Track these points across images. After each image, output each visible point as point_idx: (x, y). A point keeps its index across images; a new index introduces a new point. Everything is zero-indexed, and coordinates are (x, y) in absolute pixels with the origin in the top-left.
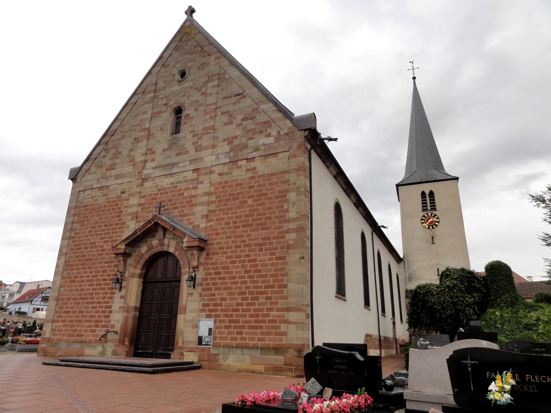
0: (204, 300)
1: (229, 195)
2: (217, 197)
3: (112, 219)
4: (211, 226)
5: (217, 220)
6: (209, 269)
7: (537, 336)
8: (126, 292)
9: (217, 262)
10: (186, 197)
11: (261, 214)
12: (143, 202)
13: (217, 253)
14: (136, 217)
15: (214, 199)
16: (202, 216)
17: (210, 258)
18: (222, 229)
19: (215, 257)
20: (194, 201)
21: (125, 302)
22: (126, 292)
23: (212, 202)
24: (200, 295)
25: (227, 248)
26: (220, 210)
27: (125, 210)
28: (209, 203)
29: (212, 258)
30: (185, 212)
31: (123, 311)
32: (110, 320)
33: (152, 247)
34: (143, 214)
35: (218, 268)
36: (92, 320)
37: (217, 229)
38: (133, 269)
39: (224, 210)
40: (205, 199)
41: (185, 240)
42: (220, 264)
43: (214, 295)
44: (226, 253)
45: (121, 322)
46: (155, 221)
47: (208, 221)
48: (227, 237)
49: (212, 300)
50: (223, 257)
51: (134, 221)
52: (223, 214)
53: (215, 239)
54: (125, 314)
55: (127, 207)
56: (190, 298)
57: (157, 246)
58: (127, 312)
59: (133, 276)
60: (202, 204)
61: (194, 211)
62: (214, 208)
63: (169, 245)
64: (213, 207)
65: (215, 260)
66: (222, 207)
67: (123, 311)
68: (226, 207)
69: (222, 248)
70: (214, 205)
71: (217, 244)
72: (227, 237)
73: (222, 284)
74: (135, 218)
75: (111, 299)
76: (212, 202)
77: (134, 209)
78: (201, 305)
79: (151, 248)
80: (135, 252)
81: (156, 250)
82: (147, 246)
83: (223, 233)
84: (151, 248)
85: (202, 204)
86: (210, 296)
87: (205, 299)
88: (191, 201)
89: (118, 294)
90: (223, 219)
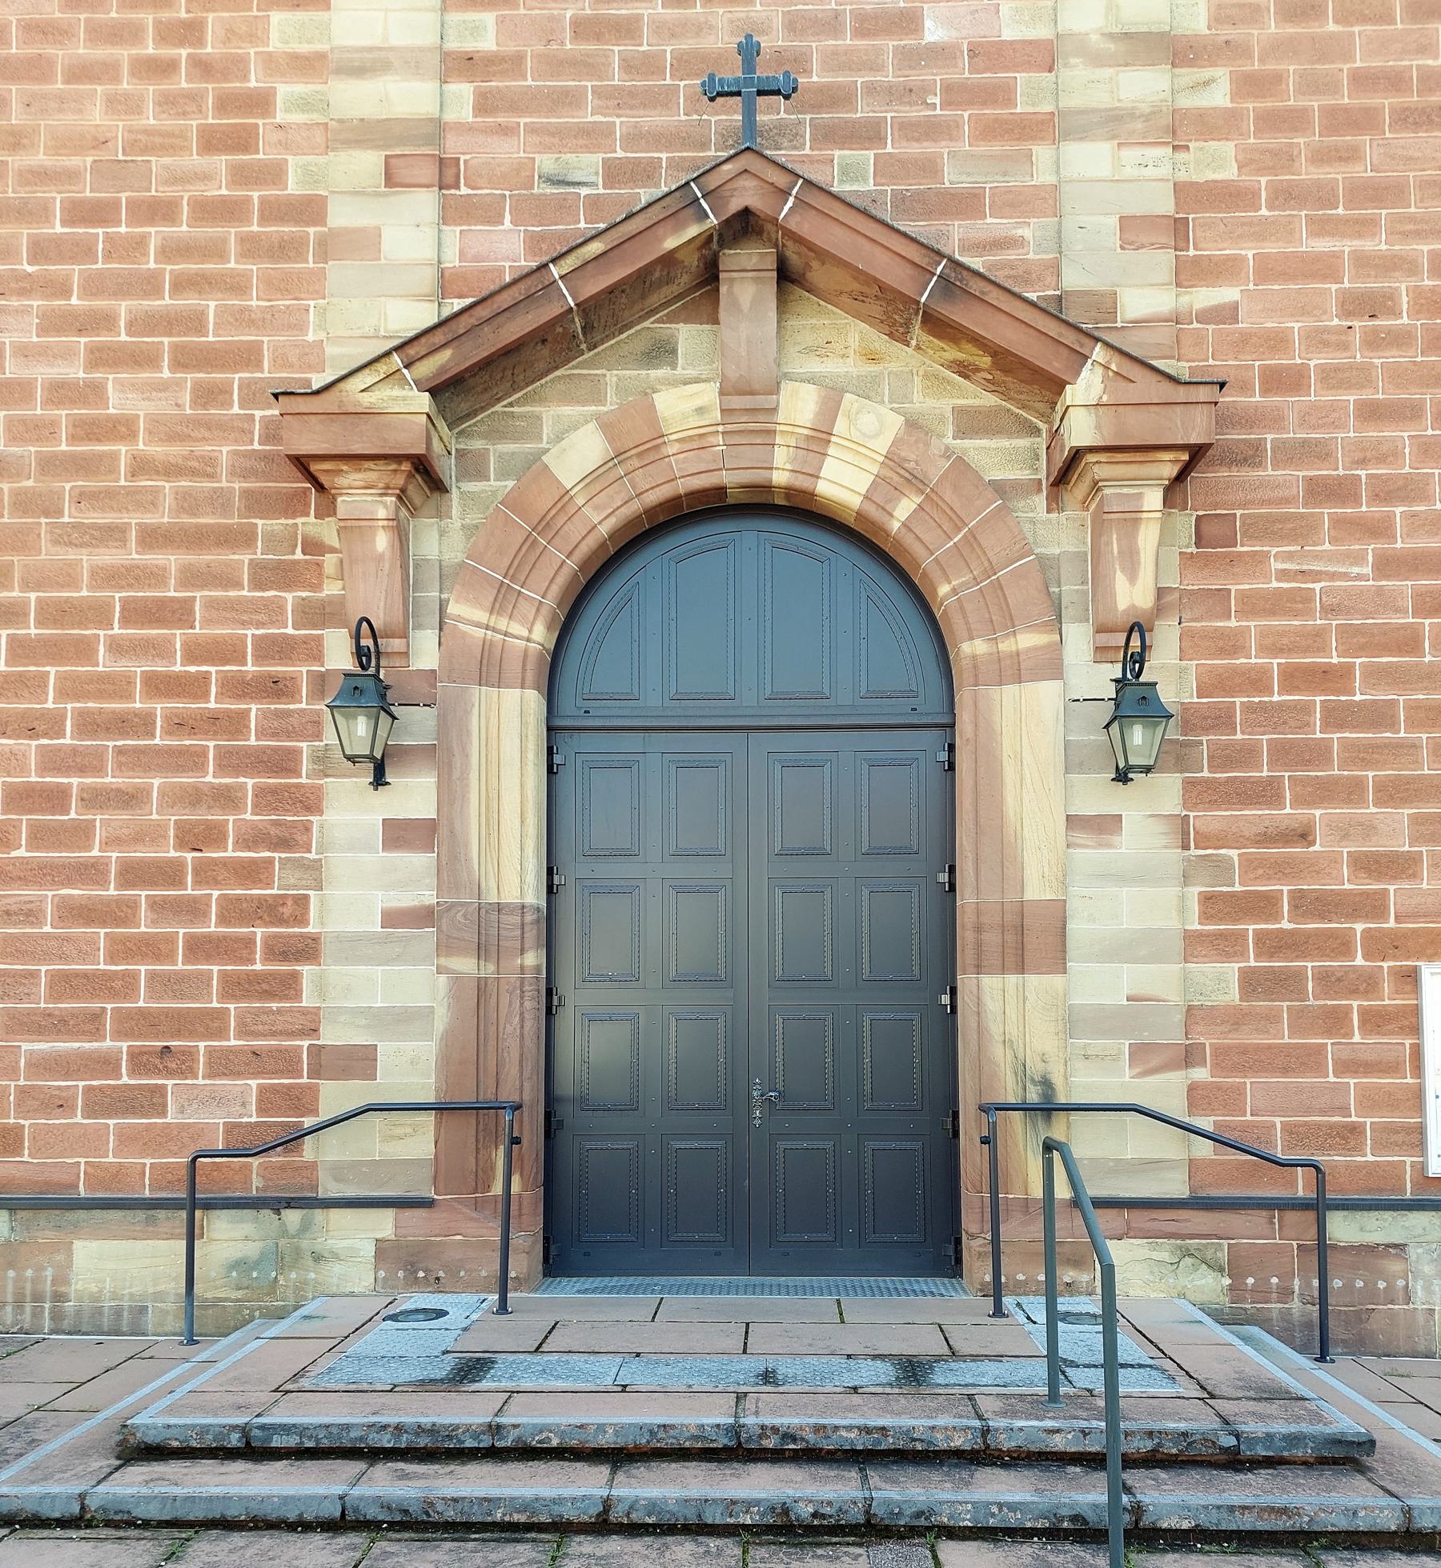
0: (1222, 868)
1: (1362, 80)
2: (1247, 85)
3: (157, 163)
4: (1227, 314)
5: (1267, 270)
6: (1231, 644)
7: (45, 1269)
8: (449, 794)
9: (1307, 597)
10: (941, 54)
11: (52, 651)
12: (487, 43)
13: (1301, 531)
14: (427, 162)
15: (1219, 96)
16: (1126, 222)
17: (1232, 560)
18: (1318, 339)
19: (1278, 557)
20: (1030, 93)
21: (450, 872)
22: (449, 794)
23: (1209, 125)
24: (1183, 834)
25: (1386, 492)
26: (1285, 196)
27: (285, 91)
28: (1178, 129)
29: (1261, 559)
30: (952, 177)
31: (445, 947)
32: (314, 1014)
33: (652, 447)
34: (508, 151)
35: (1316, 640)
36: (97, 1017)
37: (1278, 341)
38: (482, 616)
39: (1323, 196)
40: (1146, 86)
41: (1087, 387)
42: (1329, 610)
43: (1304, 836)
44: (1380, 529)
45: (441, 1020)
46: (735, 206)
47: (1187, 274)
48: (1371, 413)
49: (1282, 869)
50: (1358, 559)
51: (425, 202)
52: (1321, 227)
53: (1275, 420)
54: (466, 965)
55: (308, 65)
56: (1088, 855)
57: (697, 442)
58: (481, 951)
59: (488, 668)
60: (1114, 124)
61: (1043, 176)
62: (1230, 173)
63: (819, 439)
64: (1217, 162)
65: (1283, 575)
66: (1307, 173)
67: (445, 947)
68: (1337, 174)
69: (1338, 491)
70: (1228, 148)
71: (1290, 454)
72: (1371, 413)
73: (1359, 755)
74: (429, 172)
75: (284, 844)
76: (1209, 125)
77: (410, 97)
78: (1195, 907)
79: (638, 443)
80: (472, 466)
81: (686, 474)
82: (607, 427)
83: (1332, 377)
84: (638, 443)
85: (1114, 124)
86: (1266, 838)
87: (1224, 865)
88: (1003, 94)
89: (351, 812)
90: (1325, 268)
